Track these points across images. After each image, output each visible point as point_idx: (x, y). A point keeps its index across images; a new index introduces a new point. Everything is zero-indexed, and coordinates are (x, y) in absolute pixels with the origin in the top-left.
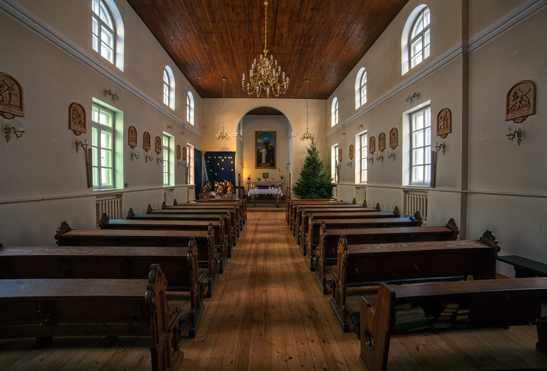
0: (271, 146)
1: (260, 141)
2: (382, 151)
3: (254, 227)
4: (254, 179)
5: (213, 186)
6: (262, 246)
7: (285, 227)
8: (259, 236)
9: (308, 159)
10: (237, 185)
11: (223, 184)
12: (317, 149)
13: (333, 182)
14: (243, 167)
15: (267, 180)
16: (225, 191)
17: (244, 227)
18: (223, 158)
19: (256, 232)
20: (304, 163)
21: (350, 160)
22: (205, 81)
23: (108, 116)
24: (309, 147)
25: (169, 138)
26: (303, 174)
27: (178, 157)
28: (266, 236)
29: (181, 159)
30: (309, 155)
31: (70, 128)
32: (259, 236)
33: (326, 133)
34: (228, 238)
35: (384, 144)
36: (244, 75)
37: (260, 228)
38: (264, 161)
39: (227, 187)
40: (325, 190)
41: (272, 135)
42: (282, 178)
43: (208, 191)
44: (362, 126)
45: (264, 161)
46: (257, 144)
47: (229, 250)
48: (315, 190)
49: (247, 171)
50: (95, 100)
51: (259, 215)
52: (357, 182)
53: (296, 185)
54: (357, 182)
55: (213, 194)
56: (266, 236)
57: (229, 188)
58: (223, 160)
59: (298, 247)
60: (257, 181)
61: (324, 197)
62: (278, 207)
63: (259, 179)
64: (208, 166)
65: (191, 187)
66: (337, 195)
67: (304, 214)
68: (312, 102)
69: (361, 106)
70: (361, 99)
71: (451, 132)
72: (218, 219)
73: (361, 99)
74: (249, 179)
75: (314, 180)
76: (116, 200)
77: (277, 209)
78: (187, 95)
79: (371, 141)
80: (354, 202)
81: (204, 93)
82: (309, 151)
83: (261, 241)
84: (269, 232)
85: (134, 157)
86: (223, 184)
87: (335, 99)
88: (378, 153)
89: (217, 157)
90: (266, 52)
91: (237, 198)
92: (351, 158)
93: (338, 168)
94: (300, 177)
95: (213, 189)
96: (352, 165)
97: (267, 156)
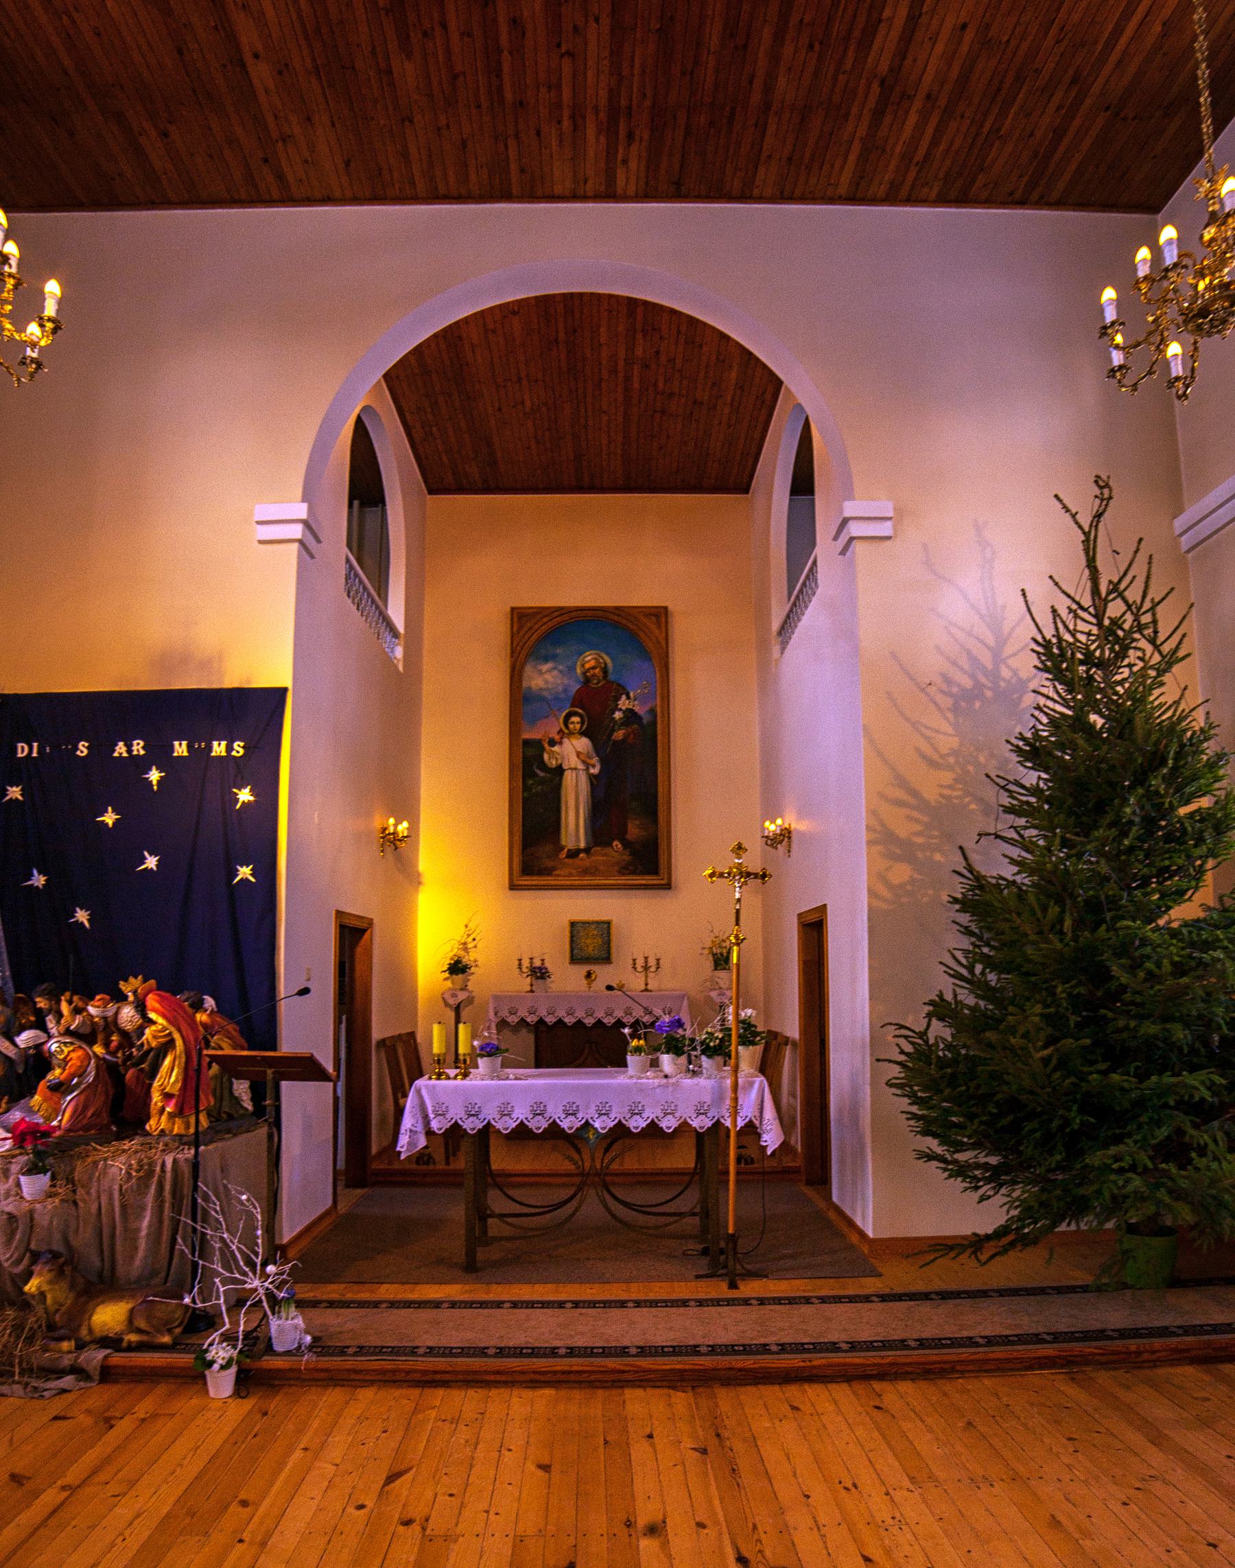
0: (631, 715)
1: (545, 678)
4: (495, 971)
14: (415, 880)
15: (605, 974)
18: (159, 754)
33: (1178, 510)
38: (574, 823)
41: (636, 634)
45: (574, 823)
46: (522, 704)
57: (169, 1075)
58: (154, 776)
74: (457, 968)
89: (102, 748)
94: (951, 940)
97: (599, 786)
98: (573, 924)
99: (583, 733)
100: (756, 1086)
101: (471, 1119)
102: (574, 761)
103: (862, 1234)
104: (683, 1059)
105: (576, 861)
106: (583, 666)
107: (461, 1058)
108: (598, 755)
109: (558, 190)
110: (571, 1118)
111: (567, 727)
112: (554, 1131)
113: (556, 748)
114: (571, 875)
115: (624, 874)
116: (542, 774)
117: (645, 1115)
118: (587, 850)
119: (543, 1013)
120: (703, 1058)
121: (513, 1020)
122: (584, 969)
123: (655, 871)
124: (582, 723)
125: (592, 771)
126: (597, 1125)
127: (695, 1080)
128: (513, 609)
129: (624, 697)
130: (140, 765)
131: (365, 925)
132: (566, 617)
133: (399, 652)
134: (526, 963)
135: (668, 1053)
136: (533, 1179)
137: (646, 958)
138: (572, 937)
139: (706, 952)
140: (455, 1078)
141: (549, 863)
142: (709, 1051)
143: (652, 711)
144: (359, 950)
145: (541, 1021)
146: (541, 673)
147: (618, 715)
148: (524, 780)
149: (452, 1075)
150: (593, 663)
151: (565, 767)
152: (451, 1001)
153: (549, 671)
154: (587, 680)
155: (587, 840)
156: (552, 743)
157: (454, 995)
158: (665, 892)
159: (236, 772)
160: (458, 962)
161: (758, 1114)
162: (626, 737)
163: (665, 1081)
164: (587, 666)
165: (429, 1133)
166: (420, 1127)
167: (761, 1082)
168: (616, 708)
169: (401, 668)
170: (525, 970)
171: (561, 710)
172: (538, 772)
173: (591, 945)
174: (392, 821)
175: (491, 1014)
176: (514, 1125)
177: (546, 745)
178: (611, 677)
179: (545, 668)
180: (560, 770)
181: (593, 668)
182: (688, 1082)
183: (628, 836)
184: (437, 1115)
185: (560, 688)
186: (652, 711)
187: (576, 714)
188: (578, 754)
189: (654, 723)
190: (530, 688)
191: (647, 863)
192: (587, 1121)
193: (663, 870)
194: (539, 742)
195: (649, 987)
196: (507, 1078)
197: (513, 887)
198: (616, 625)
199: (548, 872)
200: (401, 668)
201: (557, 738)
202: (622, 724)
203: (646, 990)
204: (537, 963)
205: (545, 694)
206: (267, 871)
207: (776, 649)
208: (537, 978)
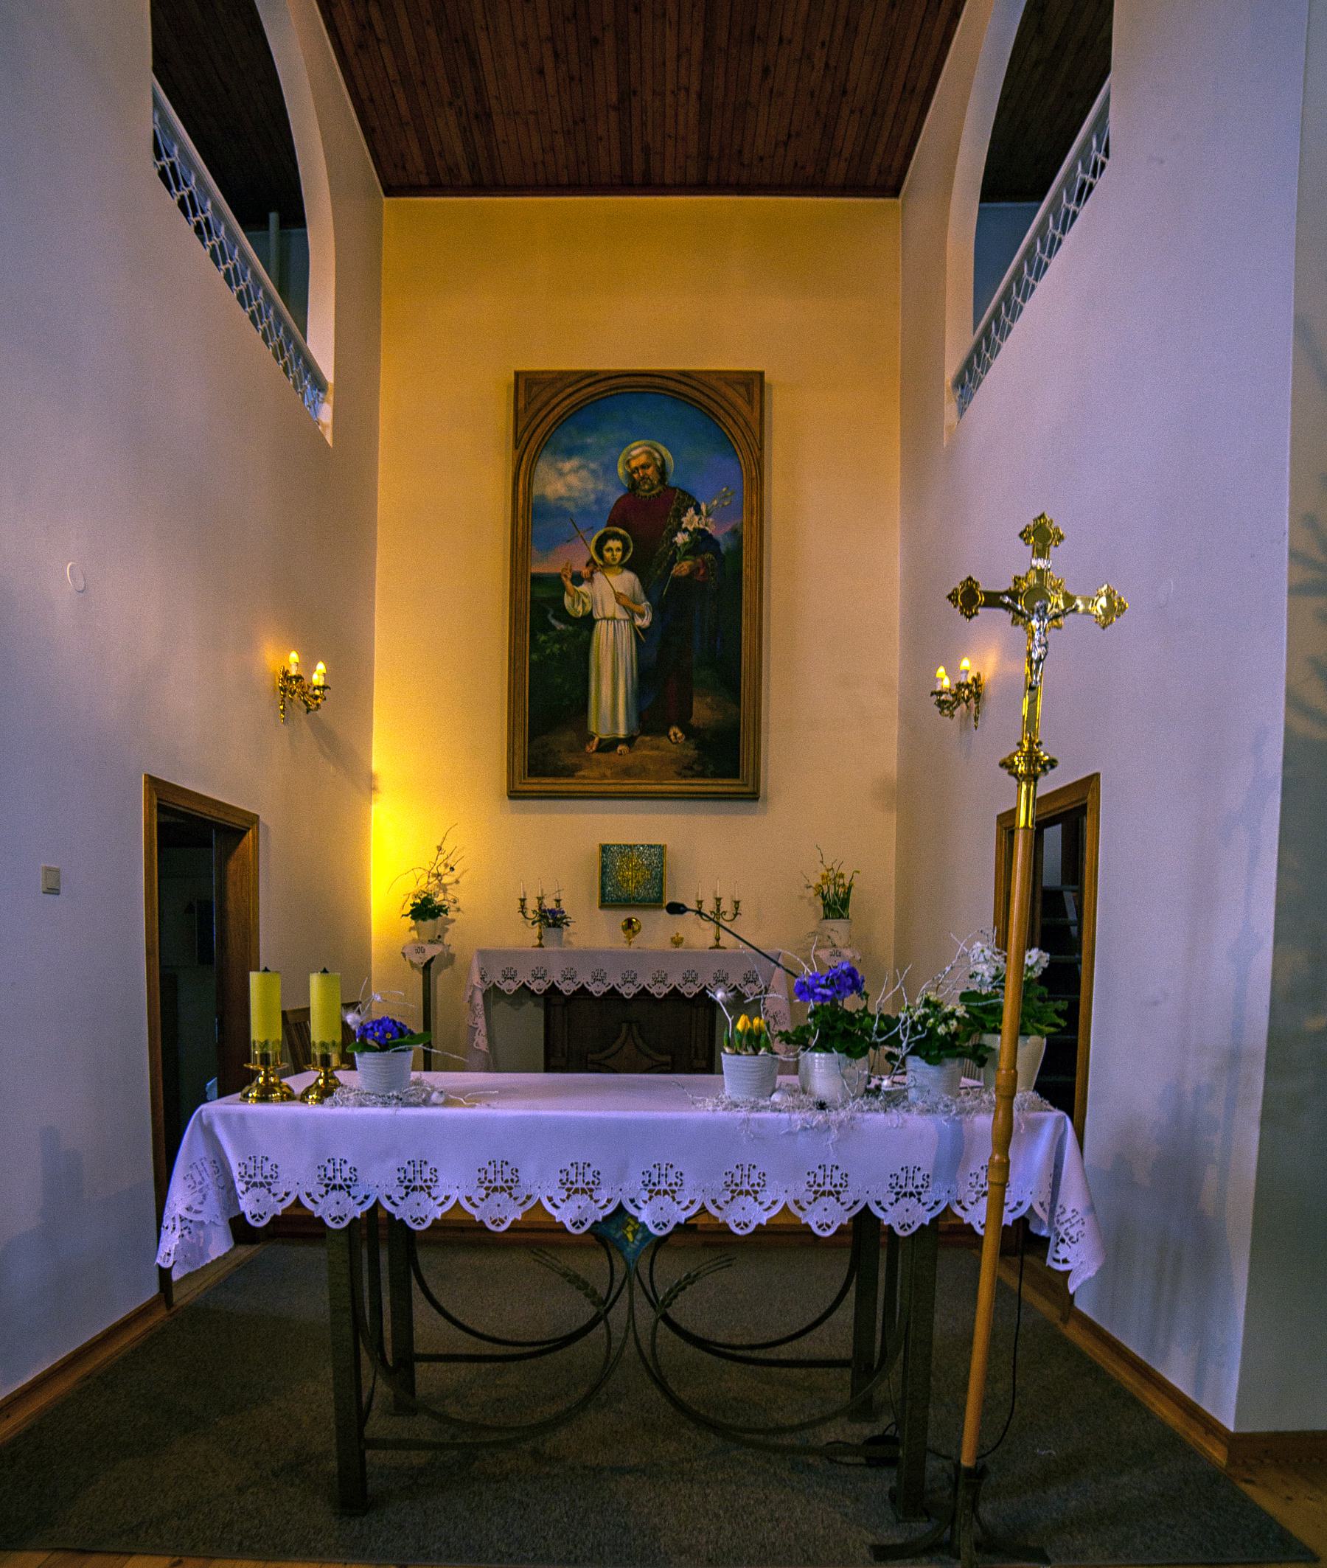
0: (702, 540)
1: (565, 481)
4: (488, 920)
14: (368, 785)
36: (330, 441)
38: (611, 699)
45: (611, 699)
46: (532, 521)
74: (425, 910)
98: (604, 849)
99: (628, 566)
100: (1047, 1131)
101: (334, 1195)
102: (611, 608)
103: (1211, 1427)
104: (860, 1067)
105: (612, 757)
106: (628, 462)
107: (317, 1052)
108: (648, 597)
110: (582, 1200)
111: (601, 556)
112: (537, 1235)
113: (583, 588)
114: (604, 776)
115: (685, 777)
116: (560, 626)
117: (766, 1196)
118: (629, 741)
119: (555, 977)
120: (915, 1063)
121: (510, 987)
122: (623, 915)
123: (734, 773)
124: (625, 549)
125: (639, 622)
126: (645, 1216)
127: (893, 1118)
128: (518, 374)
129: (691, 511)
131: (237, 822)
132: (601, 387)
133: (326, 414)
134: (532, 905)
135: (824, 1046)
136: (533, 1236)
137: (718, 900)
138: (604, 867)
139: (811, 892)
140: (303, 1098)
141: (570, 760)
142: (933, 1047)
143: (736, 534)
144: (232, 865)
145: (553, 989)
146: (561, 474)
147: (681, 538)
148: (533, 636)
149: (298, 1090)
150: (643, 459)
151: (596, 616)
152: (417, 959)
153: (575, 471)
154: (634, 486)
155: (628, 726)
156: (577, 579)
157: (420, 950)
158: (751, 804)
160: (427, 900)
161: (1046, 1197)
162: (693, 572)
163: (820, 1117)
164: (634, 464)
165: (240, 1229)
166: (212, 1212)
167: (1059, 1121)
168: (679, 528)
169: (329, 438)
170: (530, 914)
171: (592, 529)
172: (553, 621)
173: (633, 886)
174: (294, 657)
175: (476, 978)
176: (439, 1213)
177: (568, 584)
178: (672, 480)
179: (567, 466)
180: (588, 622)
181: (644, 467)
182: (878, 1119)
183: (693, 721)
184: (251, 1185)
185: (592, 497)
186: (736, 534)
187: (616, 536)
188: (618, 597)
189: (737, 552)
190: (543, 497)
192: (620, 1209)
193: (746, 768)
194: (559, 577)
195: (721, 943)
196: (426, 1103)
197: (514, 795)
198: (678, 398)
199: (569, 772)
200: (329, 438)
201: (585, 571)
202: (687, 552)
203: (718, 947)
204: (549, 904)
205: (571, 507)
207: (950, 408)
208: (549, 926)
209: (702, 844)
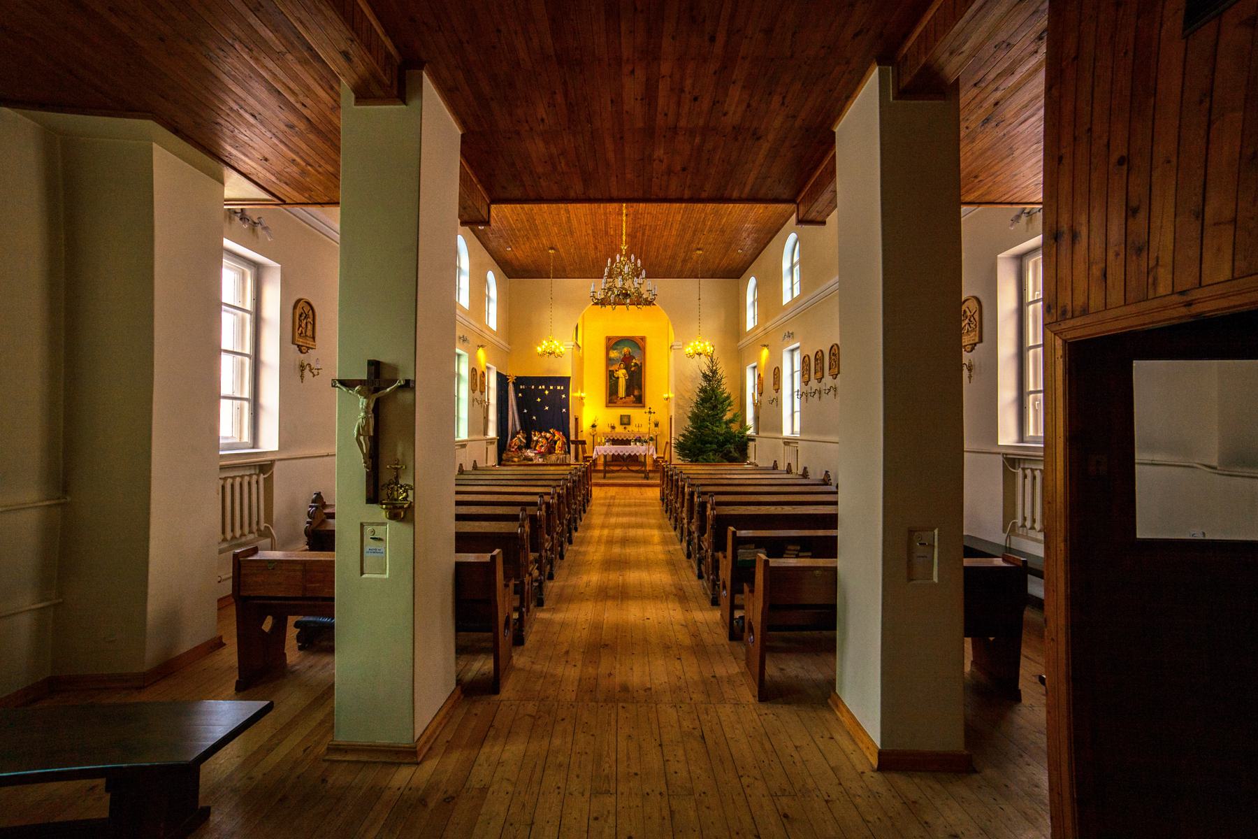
1: (614, 354)
2: (820, 380)
3: (604, 509)
4: (603, 427)
5: (529, 439)
6: (618, 532)
7: (658, 507)
8: (613, 520)
9: (703, 390)
10: (572, 438)
11: (548, 435)
12: (719, 372)
13: (748, 433)
16: (551, 450)
17: (588, 509)
19: (607, 515)
20: (695, 398)
21: (774, 395)
22: (519, 253)
23: (243, 274)
24: (705, 369)
25: (258, 268)
26: (695, 418)
27: (473, 388)
28: (624, 520)
29: (478, 392)
30: (704, 384)
31: (293, 343)
32: (613, 520)
34: (538, 560)
35: (822, 369)
37: (615, 510)
38: (622, 392)
39: (555, 442)
40: (736, 448)
41: (637, 344)
42: (656, 425)
43: (520, 448)
44: (790, 335)
45: (622, 392)
46: (609, 361)
47: (540, 588)
48: (715, 446)
49: (591, 412)
50: (228, 243)
51: (612, 491)
52: (786, 432)
53: (681, 439)
54: (786, 432)
55: (530, 453)
56: (624, 520)
57: (559, 444)
59: (673, 533)
60: (609, 430)
61: (732, 460)
62: (647, 478)
63: (613, 428)
64: (520, 404)
65: (490, 442)
66: (759, 454)
67: (712, 509)
68: (708, 286)
69: (793, 299)
70: (790, 289)
71: (981, 341)
72: (514, 518)
73: (790, 289)
74: (594, 426)
75: (713, 430)
76: (255, 477)
77: (645, 481)
78: (486, 280)
79: (805, 361)
80: (775, 467)
81: (511, 270)
82: (705, 376)
83: (616, 526)
84: (630, 514)
85: (307, 371)
86: (548, 435)
87: (752, 282)
88: (814, 384)
89: (537, 387)
90: (624, 247)
91: (573, 461)
92: (777, 391)
93: (757, 407)
95: (529, 444)
96: (777, 402)
109: (615, 193)
130: (543, 391)
159: (561, 392)
173: (626, 421)
191: (639, 401)
206: (568, 410)
209: (637, 414)
